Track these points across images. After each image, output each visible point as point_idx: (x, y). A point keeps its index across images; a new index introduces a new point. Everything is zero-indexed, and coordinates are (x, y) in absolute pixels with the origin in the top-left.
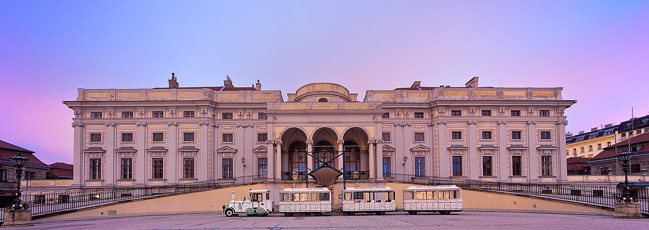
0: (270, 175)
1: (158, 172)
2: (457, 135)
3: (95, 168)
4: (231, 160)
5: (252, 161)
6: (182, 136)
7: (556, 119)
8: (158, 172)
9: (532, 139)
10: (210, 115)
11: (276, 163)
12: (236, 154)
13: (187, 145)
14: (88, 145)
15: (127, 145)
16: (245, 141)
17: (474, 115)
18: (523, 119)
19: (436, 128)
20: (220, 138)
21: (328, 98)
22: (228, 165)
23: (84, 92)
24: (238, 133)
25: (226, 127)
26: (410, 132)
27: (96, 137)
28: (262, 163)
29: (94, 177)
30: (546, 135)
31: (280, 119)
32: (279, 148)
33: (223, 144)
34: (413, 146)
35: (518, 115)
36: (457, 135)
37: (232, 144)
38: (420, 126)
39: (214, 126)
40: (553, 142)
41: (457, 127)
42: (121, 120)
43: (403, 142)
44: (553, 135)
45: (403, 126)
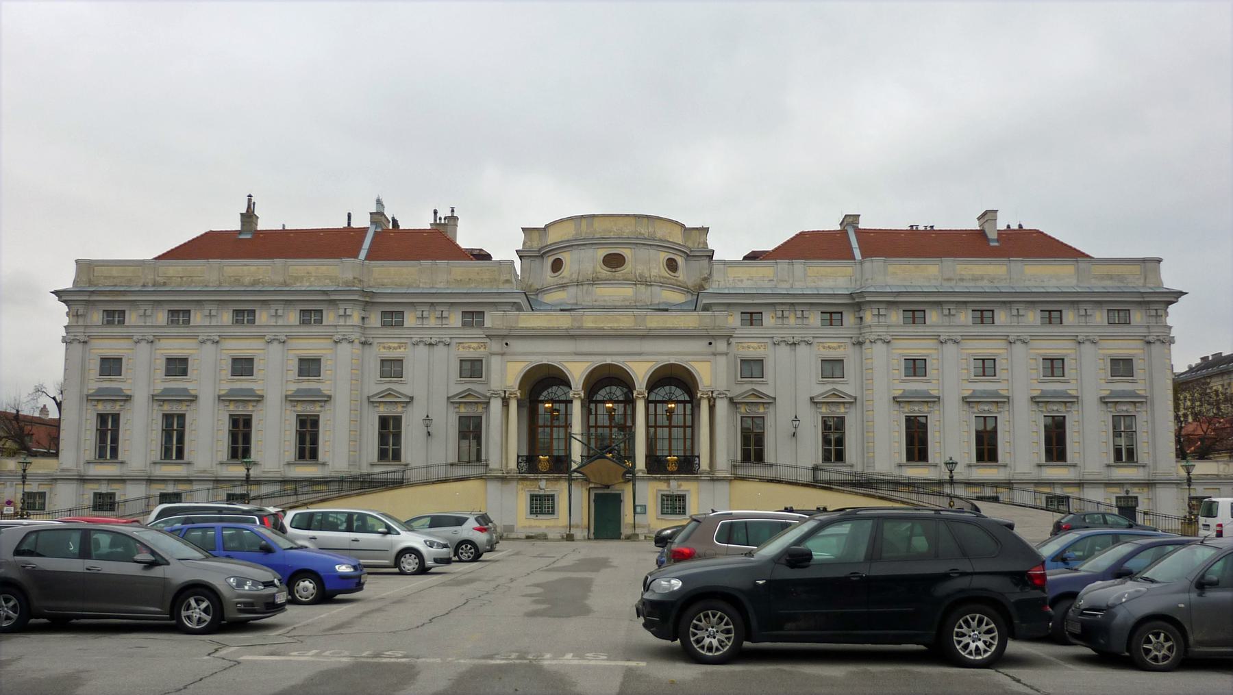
0: (494, 462)
1: (308, 447)
2: (916, 367)
3: (108, 434)
4: (398, 420)
5: (447, 424)
6: (161, 365)
7: (1143, 331)
8: (308, 447)
9: (1089, 377)
10: (355, 319)
11: (505, 438)
12: (409, 408)
13: (305, 386)
14: (95, 383)
15: (177, 383)
16: (430, 381)
17: (427, 324)
18: (1000, 330)
19: (868, 350)
20: (374, 368)
21: (626, 252)
22: (390, 429)
23: (84, 267)
24: (416, 360)
25: (388, 345)
26: (808, 360)
27: (111, 366)
28: (471, 430)
29: (101, 455)
30: (1122, 367)
31: (517, 346)
32: (513, 405)
33: (380, 383)
34: (818, 390)
35: (122, 322)
36: (916, 367)
37: (402, 383)
38: (835, 344)
39: (364, 343)
40: (1138, 386)
41: (916, 349)
42: (166, 330)
43: (793, 381)
44: (1138, 365)
45: (430, 344)
